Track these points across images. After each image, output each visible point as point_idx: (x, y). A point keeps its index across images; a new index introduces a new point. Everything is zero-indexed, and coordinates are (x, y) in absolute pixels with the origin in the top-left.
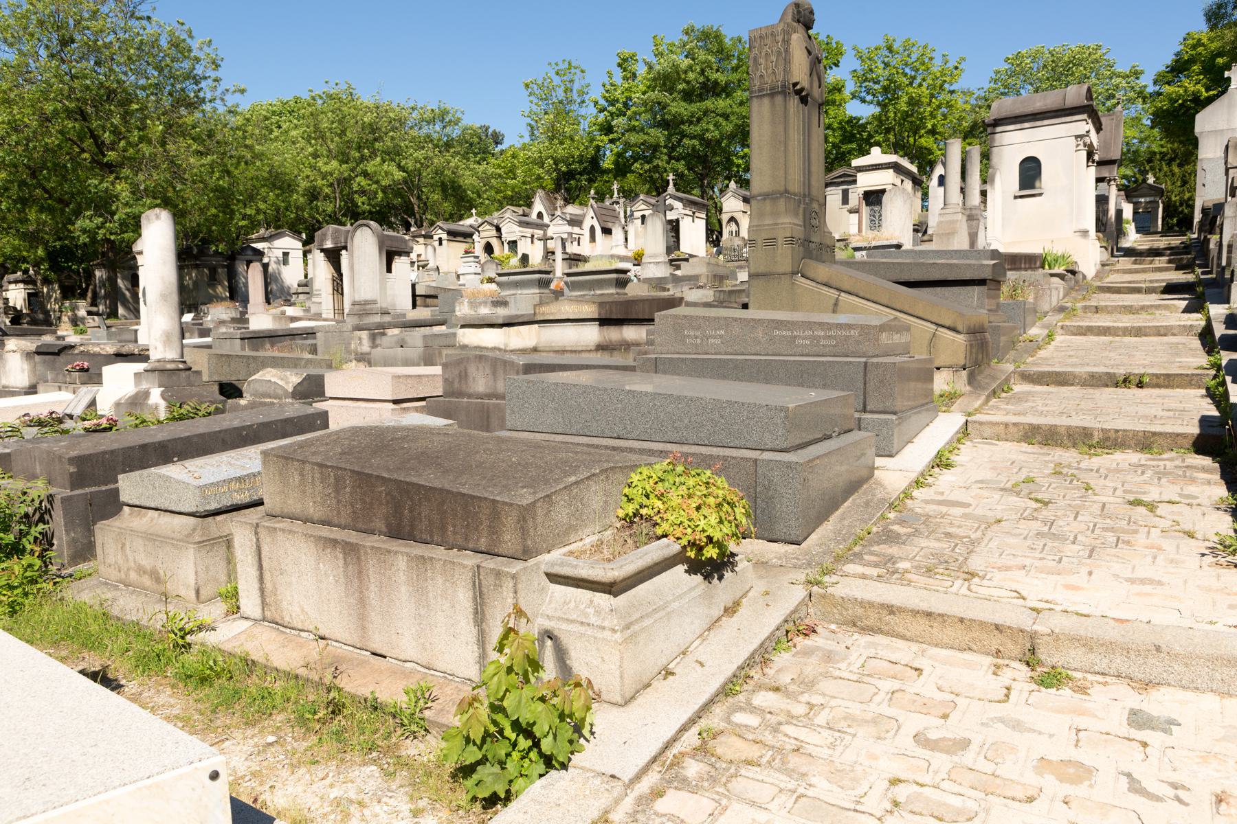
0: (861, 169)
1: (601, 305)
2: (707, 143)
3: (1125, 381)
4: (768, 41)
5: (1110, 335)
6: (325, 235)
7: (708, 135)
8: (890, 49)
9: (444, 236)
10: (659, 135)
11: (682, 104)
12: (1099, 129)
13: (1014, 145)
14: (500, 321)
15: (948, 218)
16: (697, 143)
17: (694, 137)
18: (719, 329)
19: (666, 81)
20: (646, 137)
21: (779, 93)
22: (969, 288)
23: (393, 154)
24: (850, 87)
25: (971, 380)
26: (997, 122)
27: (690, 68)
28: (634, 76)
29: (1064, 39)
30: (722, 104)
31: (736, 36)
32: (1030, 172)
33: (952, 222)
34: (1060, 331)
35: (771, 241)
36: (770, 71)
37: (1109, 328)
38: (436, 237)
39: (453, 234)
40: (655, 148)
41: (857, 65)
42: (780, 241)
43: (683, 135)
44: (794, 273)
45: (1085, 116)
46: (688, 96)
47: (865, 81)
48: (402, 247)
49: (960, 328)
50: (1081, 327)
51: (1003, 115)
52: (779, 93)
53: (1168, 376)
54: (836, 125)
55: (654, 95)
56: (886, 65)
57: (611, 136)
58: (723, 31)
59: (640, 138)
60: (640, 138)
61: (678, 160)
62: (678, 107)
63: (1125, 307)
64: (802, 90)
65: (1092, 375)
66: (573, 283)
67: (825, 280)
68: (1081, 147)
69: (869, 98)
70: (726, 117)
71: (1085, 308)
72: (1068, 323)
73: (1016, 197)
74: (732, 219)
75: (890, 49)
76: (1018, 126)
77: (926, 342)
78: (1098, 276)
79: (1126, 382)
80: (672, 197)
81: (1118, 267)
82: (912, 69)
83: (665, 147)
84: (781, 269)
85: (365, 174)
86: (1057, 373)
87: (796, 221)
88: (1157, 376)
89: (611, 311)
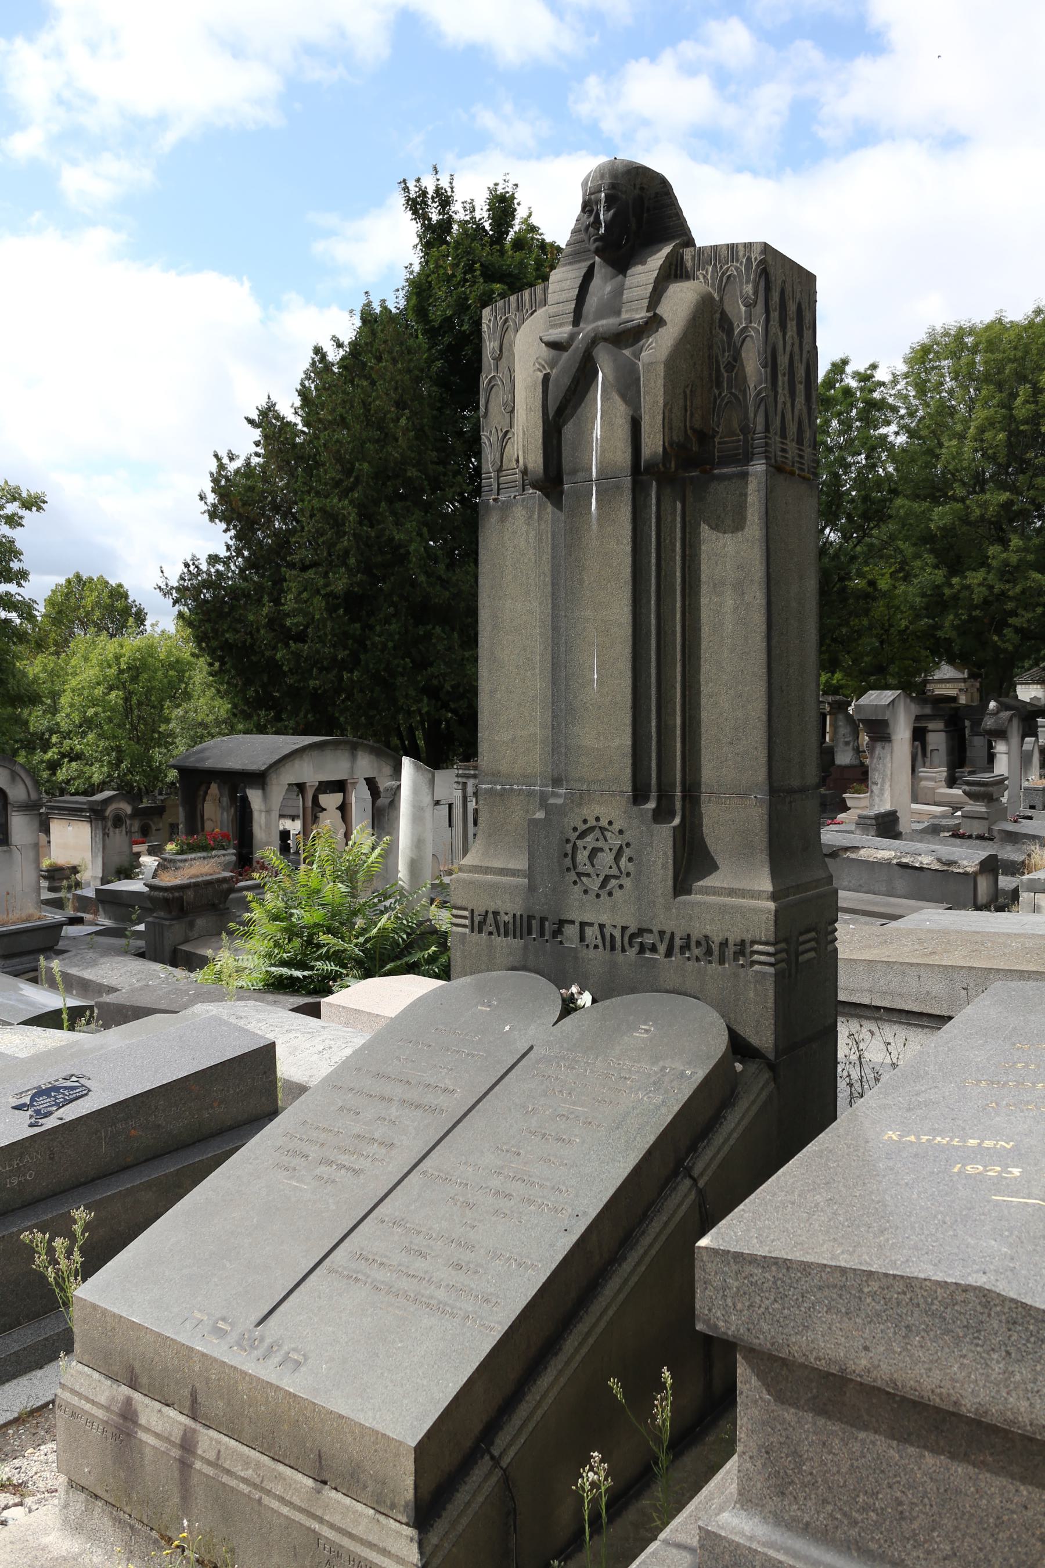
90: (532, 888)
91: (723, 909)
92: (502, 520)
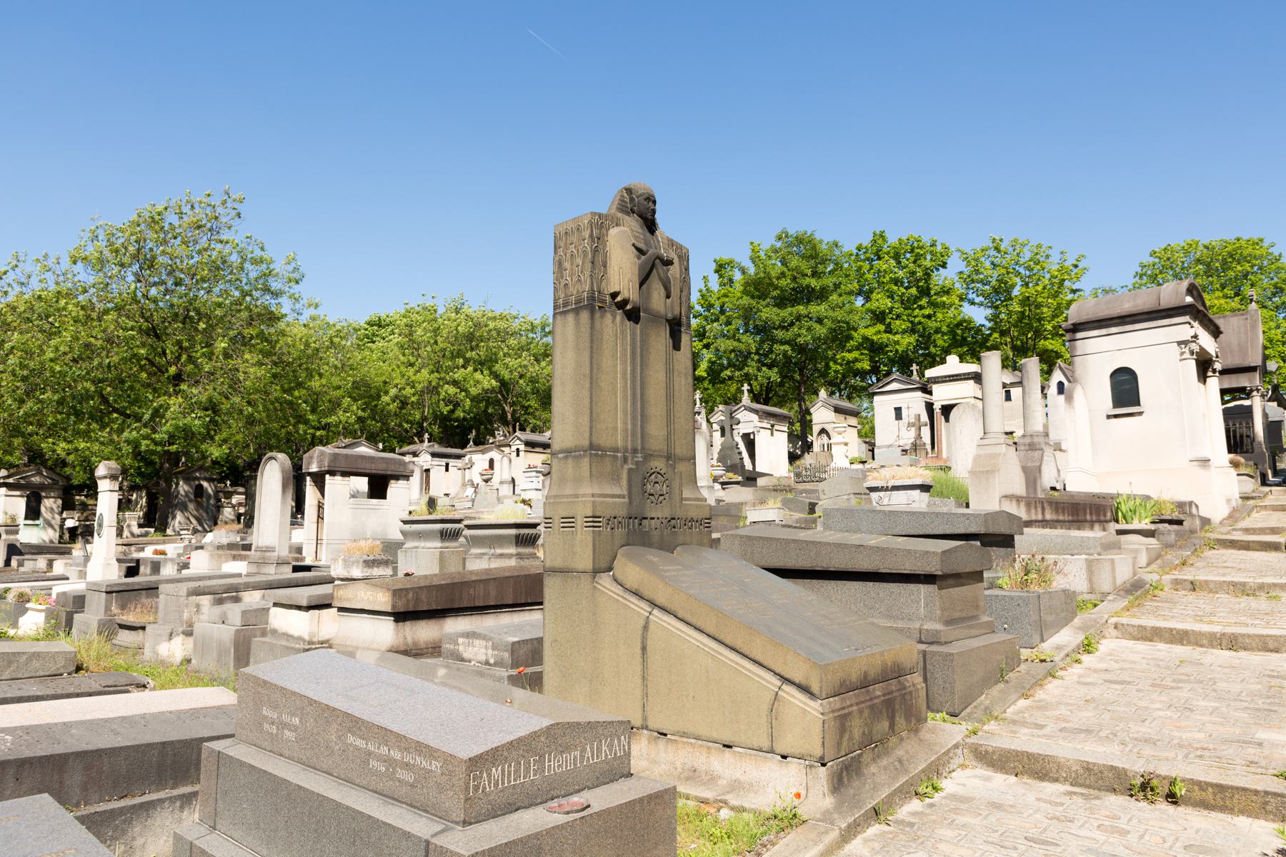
0: (937, 380)
1: (397, 593)
2: (801, 349)
3: (1145, 786)
4: (574, 239)
5: (1189, 643)
6: (311, 457)
7: (801, 340)
8: (997, 249)
9: (522, 447)
10: (750, 342)
11: (775, 309)
12: (1216, 332)
13: (1100, 355)
14: (304, 604)
15: (989, 450)
16: (787, 347)
17: (786, 343)
18: (293, 715)
19: (758, 288)
20: (735, 344)
21: (584, 307)
22: (912, 586)
23: (486, 364)
24: (959, 287)
25: (838, 783)
26: (1076, 328)
27: (783, 274)
28: (731, 281)
29: (1214, 228)
30: (816, 309)
31: (831, 240)
32: (1125, 389)
33: (993, 456)
34: (1114, 633)
35: (569, 521)
36: (575, 279)
37: (1186, 633)
38: (514, 448)
39: (531, 445)
40: (747, 356)
41: (962, 266)
42: (580, 522)
43: (774, 341)
44: (596, 572)
45: (1187, 318)
46: (781, 303)
47: (973, 281)
48: (400, 470)
49: (815, 688)
50: (1145, 628)
51: (1084, 318)
52: (584, 307)
53: (1221, 788)
54: (944, 329)
55: (746, 301)
56: (994, 265)
57: (705, 341)
58: (818, 237)
59: (731, 344)
60: (731, 344)
61: (770, 367)
62: (768, 313)
63: (1234, 584)
64: (626, 302)
65: (1088, 768)
66: (473, 537)
67: (635, 586)
68: (1187, 355)
69: (978, 300)
70: (820, 321)
71: (1177, 583)
72: (1124, 620)
73: (1109, 417)
74: (823, 431)
75: (997, 249)
76: (1104, 331)
77: (765, 707)
78: (1233, 516)
79: (1145, 788)
80: (747, 408)
81: (1266, 502)
82: (1026, 268)
83: (757, 353)
84: (581, 566)
85: (455, 383)
86: (1030, 756)
87: (617, 491)
88: (1203, 786)
89: (417, 600)
90: (630, 503)
91: (697, 506)
92: (602, 317)
